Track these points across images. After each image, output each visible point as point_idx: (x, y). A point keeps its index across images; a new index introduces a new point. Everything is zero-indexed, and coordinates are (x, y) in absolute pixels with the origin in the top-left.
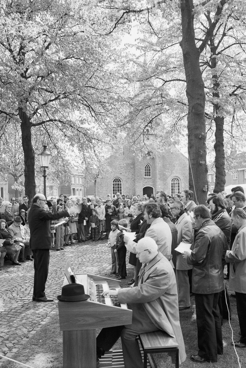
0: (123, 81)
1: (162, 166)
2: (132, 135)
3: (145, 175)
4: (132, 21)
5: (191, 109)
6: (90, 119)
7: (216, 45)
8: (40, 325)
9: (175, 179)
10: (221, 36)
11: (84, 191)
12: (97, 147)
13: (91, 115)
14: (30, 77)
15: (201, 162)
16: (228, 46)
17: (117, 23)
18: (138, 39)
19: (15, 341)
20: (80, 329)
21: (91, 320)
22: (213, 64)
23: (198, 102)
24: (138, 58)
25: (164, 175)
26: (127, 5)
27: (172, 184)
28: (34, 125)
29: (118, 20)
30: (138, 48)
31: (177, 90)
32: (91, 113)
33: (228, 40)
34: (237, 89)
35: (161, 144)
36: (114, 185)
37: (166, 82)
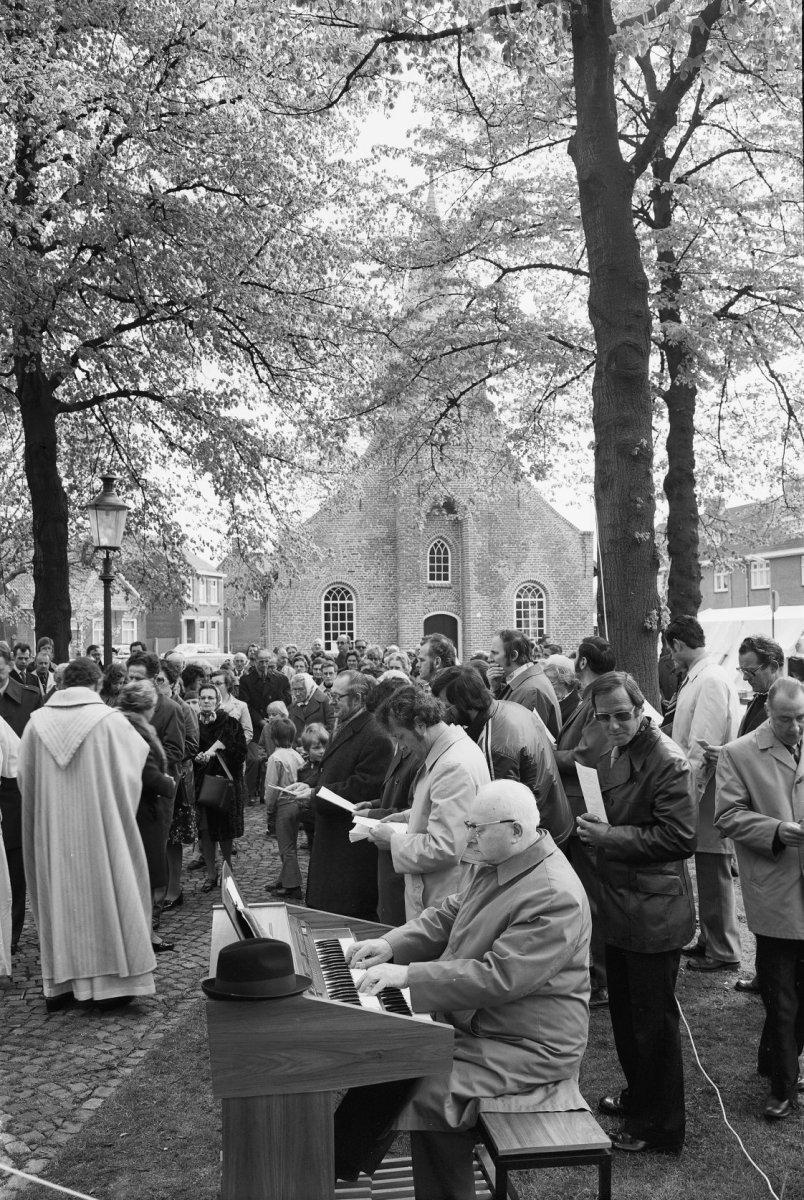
0: (367, 268)
1: (486, 549)
2: (391, 445)
3: (432, 577)
4: (404, 67)
5: (605, 361)
6: (253, 390)
7: (670, 155)
8: (114, 1077)
9: (529, 590)
10: (687, 125)
11: (226, 627)
12: (277, 481)
13: (255, 377)
14: (53, 248)
15: (637, 535)
16: (707, 159)
17: (354, 73)
18: (415, 131)
19: (35, 1135)
20: (278, 1091)
21: (316, 1062)
22: (663, 220)
23: (630, 338)
24: (415, 193)
25: (493, 576)
26: (387, 15)
27: (519, 605)
28: (67, 408)
29: (359, 61)
30: (416, 161)
31: (555, 295)
32: (257, 372)
33: (708, 140)
34: (737, 298)
35: (490, 474)
36: (327, 607)
37: (506, 271)
